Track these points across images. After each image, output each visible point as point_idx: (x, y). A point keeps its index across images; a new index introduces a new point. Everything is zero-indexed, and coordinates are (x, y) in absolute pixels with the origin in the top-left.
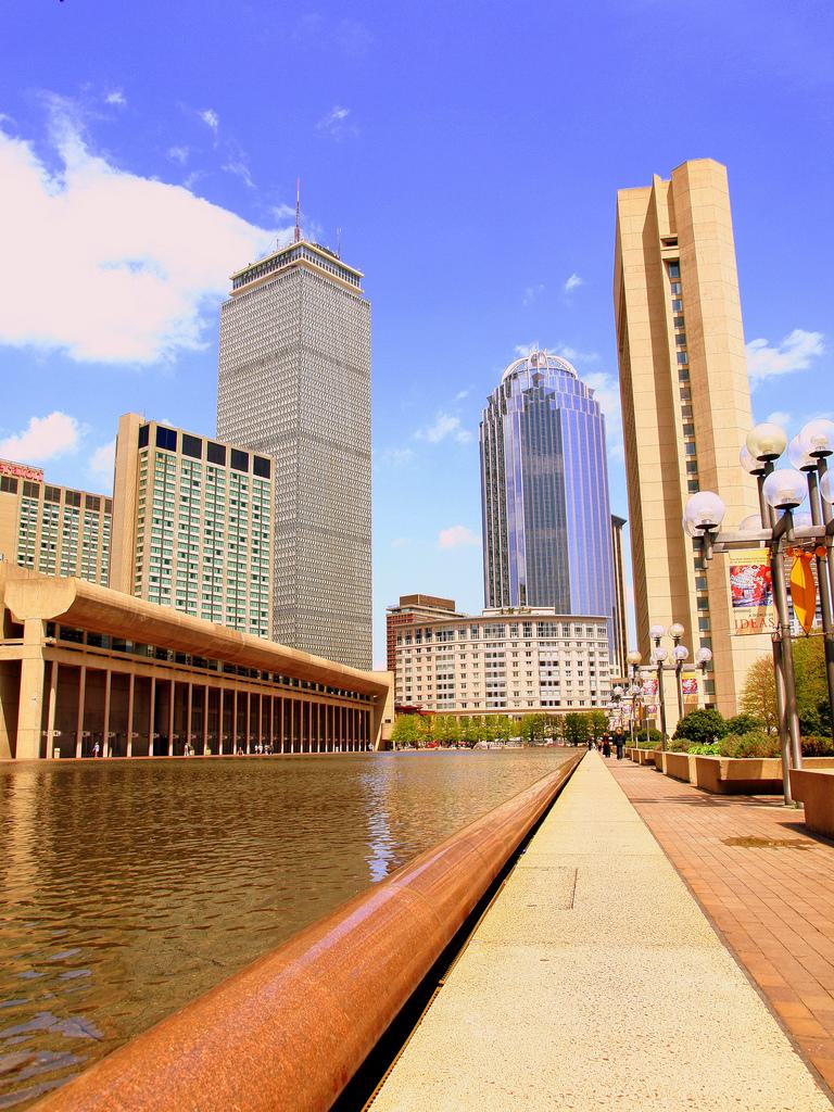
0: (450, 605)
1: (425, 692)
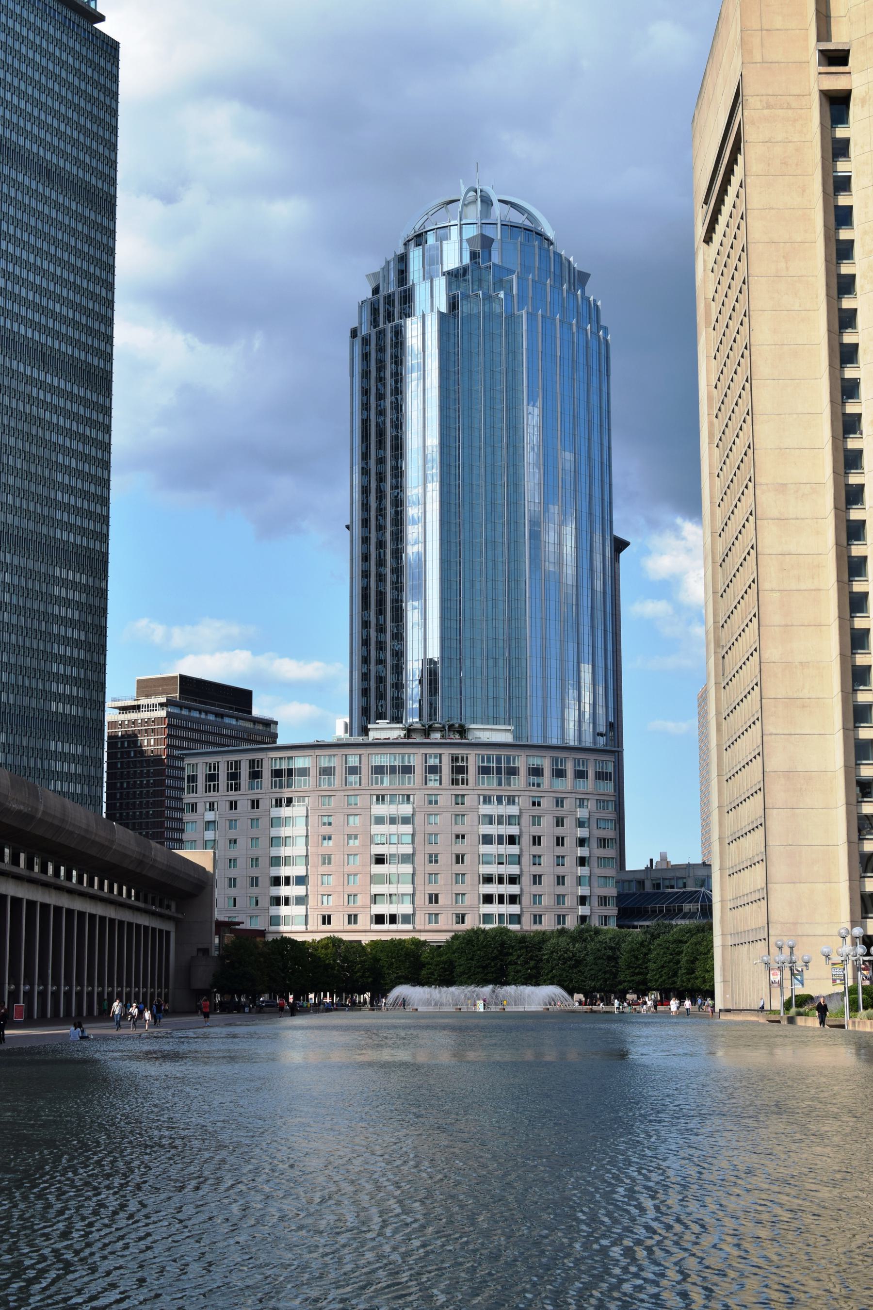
0: (240, 699)
1: (242, 891)
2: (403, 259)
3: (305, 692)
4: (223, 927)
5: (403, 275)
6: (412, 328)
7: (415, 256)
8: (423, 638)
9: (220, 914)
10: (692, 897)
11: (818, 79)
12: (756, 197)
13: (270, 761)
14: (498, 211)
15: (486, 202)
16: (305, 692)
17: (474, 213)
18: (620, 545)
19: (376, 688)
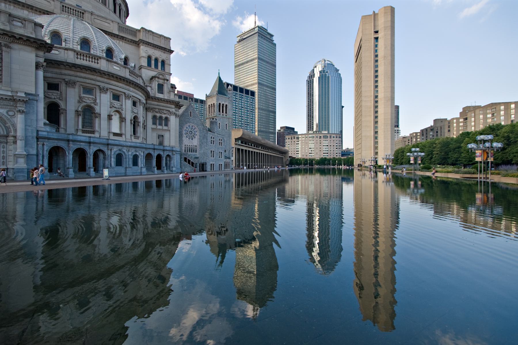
0: (293, 129)
1: (293, 153)
2: (313, 70)
3: (301, 128)
4: (290, 157)
5: (313, 72)
6: (315, 79)
7: (315, 69)
8: (316, 121)
9: (290, 155)
10: (352, 153)
11: (373, 36)
12: (363, 55)
13: (296, 137)
14: (327, 62)
15: (325, 61)
16: (301, 128)
17: (323, 62)
18: (343, 107)
19: (310, 126)
